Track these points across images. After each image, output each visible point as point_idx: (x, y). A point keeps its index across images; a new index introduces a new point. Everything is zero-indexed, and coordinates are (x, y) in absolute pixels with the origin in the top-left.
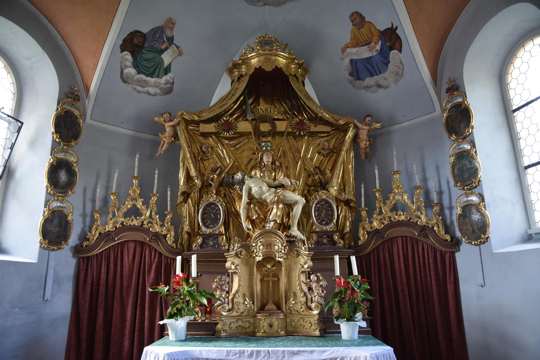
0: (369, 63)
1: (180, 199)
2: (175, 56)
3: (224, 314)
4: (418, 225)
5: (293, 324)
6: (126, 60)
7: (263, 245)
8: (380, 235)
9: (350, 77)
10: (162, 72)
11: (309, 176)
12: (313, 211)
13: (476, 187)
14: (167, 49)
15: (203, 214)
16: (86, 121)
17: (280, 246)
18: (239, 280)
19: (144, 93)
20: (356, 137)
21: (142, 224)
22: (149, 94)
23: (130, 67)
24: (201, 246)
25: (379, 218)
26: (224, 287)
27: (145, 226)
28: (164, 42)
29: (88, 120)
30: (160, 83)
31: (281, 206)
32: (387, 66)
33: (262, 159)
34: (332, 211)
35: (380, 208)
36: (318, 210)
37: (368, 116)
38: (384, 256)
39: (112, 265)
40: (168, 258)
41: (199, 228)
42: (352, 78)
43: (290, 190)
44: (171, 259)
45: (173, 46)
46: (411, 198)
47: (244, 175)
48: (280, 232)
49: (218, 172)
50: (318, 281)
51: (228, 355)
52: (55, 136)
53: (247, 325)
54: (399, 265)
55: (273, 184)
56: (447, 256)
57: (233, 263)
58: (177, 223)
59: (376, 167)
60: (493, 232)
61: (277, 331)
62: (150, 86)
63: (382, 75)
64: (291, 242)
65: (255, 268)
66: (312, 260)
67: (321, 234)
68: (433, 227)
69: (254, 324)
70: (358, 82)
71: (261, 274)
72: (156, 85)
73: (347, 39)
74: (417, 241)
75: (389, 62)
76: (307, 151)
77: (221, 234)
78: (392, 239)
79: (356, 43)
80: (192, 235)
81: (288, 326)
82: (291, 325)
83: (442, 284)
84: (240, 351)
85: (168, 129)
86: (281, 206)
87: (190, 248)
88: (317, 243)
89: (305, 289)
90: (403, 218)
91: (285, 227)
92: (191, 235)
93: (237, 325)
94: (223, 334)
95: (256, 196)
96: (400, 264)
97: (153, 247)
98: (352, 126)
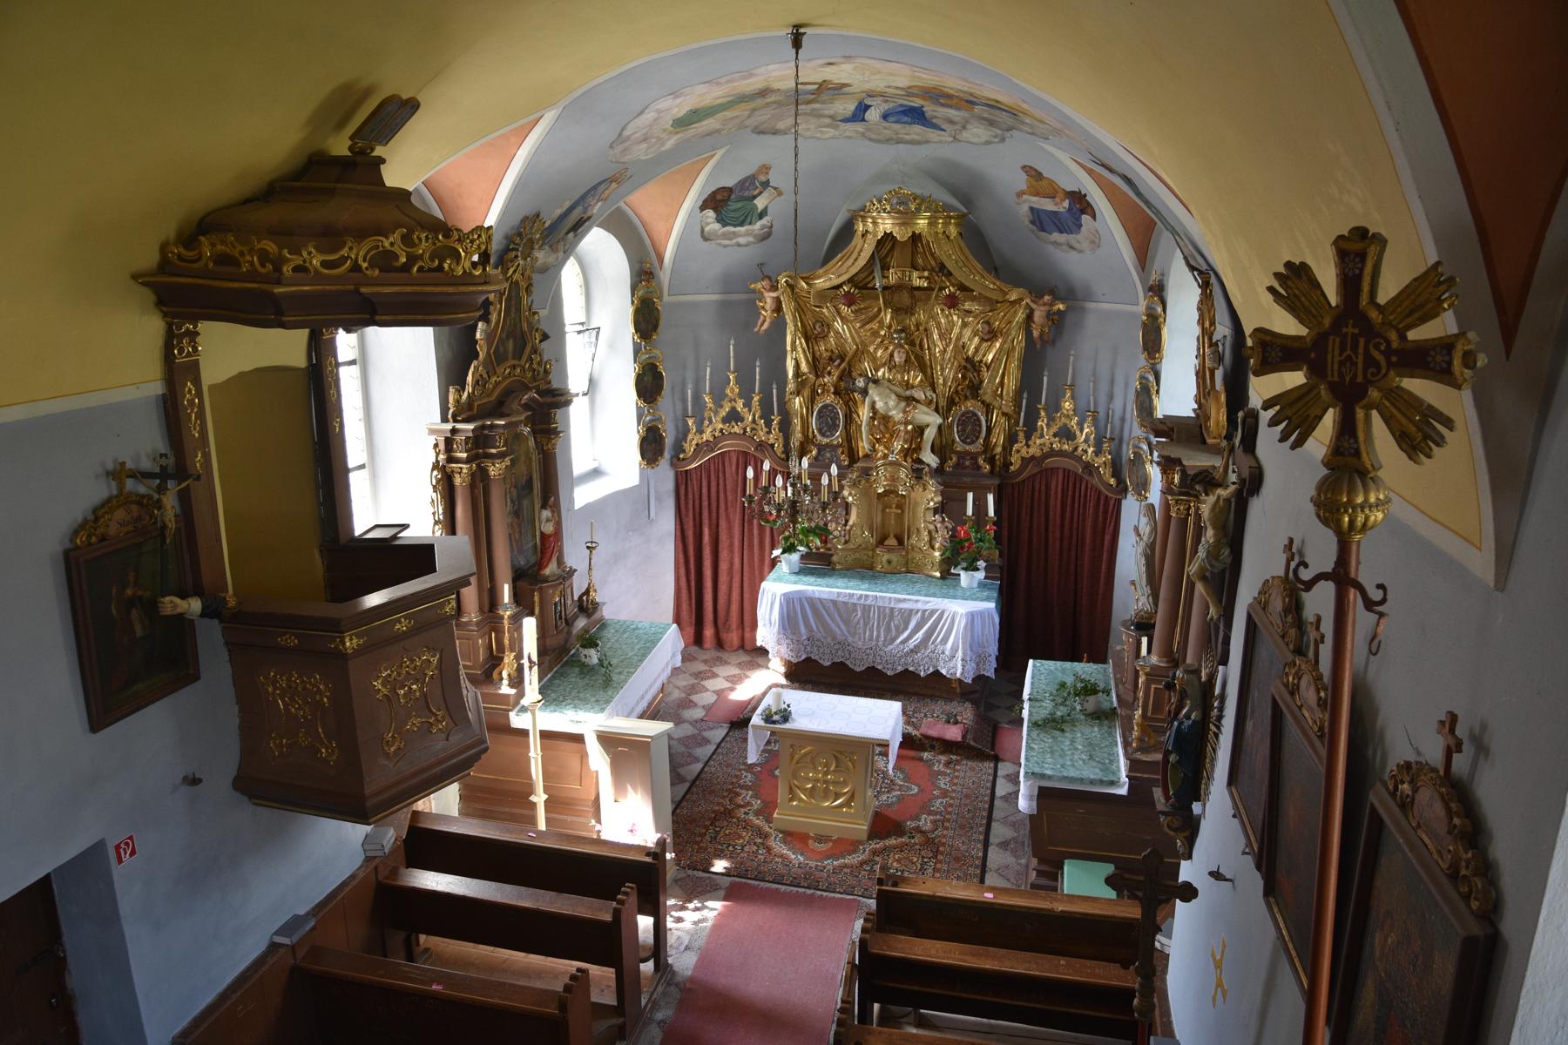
2: (772, 198)
3: (839, 547)
4: (1082, 460)
6: (708, 217)
9: (1030, 225)
14: (761, 193)
19: (733, 246)
21: (745, 431)
22: (739, 245)
28: (757, 187)
29: (666, 298)
30: (753, 231)
32: (1080, 229)
35: (1043, 429)
41: (814, 436)
42: (1034, 228)
51: (838, 596)
55: (903, 394)
56: (1112, 502)
62: (741, 236)
63: (1074, 236)
68: (1099, 467)
72: (747, 234)
74: (1081, 479)
78: (1052, 469)
84: (850, 594)
86: (910, 427)
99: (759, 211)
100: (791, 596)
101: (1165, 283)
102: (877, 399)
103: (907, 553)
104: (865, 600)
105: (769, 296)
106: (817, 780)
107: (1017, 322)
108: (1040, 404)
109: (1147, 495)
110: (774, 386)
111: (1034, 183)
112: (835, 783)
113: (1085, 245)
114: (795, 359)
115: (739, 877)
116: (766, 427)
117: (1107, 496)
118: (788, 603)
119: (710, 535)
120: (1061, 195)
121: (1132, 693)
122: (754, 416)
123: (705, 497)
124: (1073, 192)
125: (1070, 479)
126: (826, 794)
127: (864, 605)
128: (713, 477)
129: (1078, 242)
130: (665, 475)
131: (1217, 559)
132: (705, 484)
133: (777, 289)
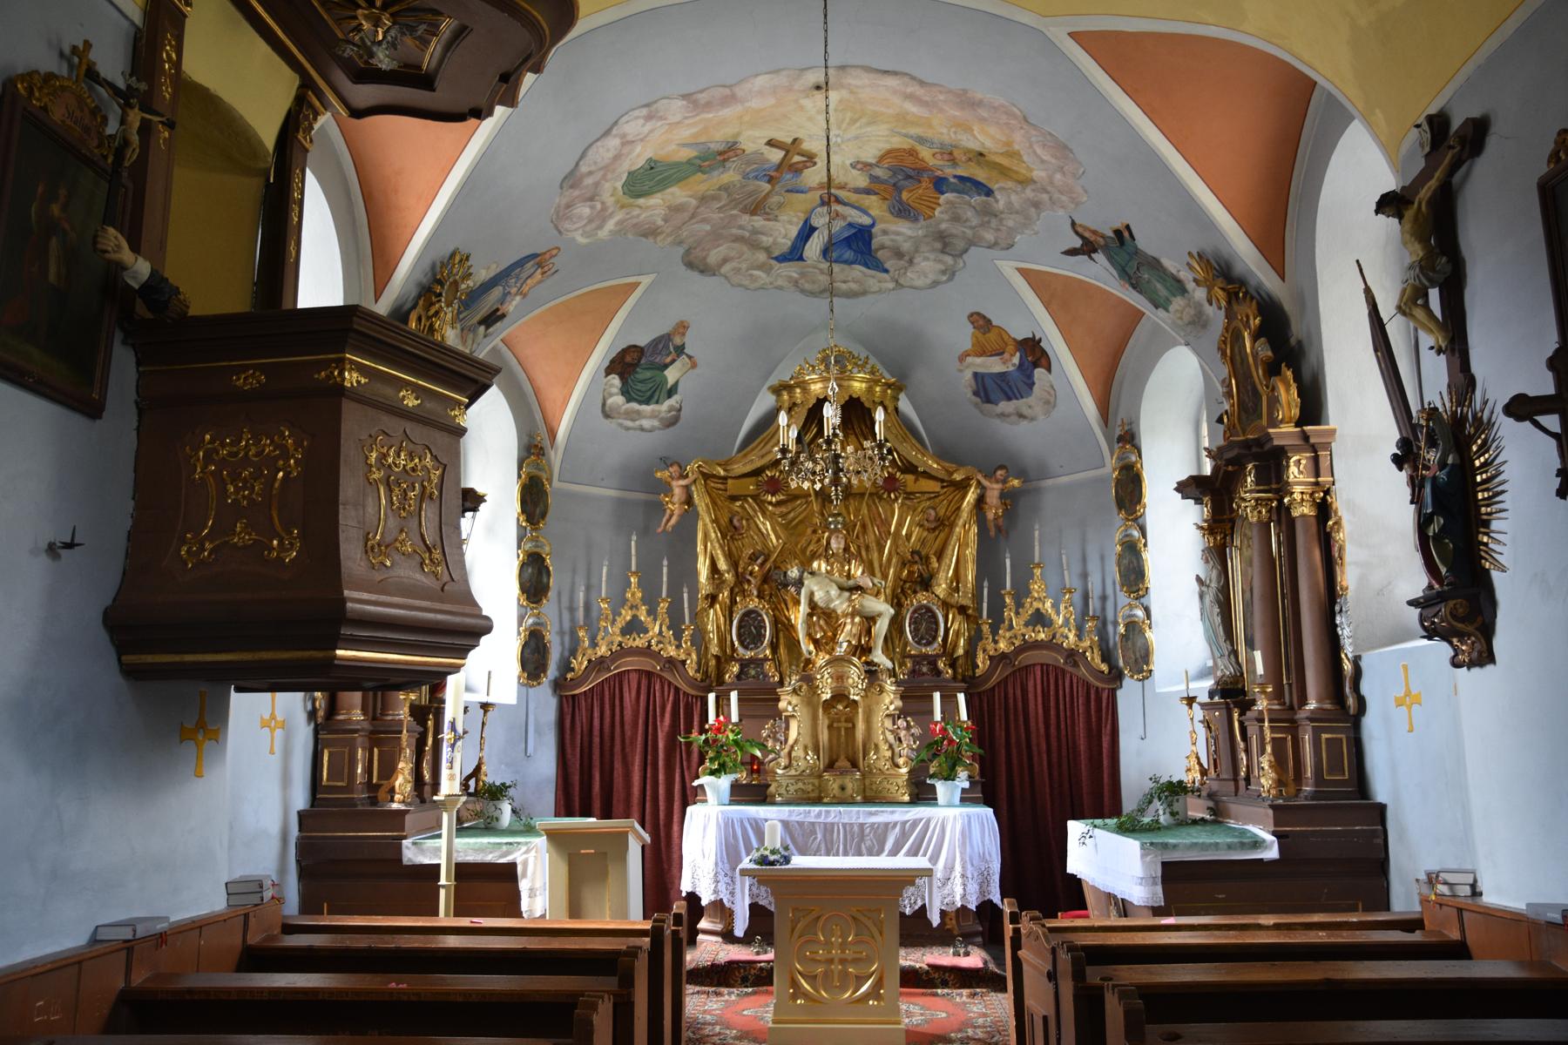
0: (1003, 381)
1: (702, 604)
3: (779, 771)
5: (874, 787)
6: (612, 386)
7: (832, 677)
8: (1008, 661)
9: (973, 398)
10: (664, 394)
11: (904, 564)
12: (907, 624)
13: (1143, 596)
14: (673, 361)
15: (740, 627)
16: (553, 484)
17: (856, 679)
18: (799, 726)
19: (634, 429)
20: (980, 501)
21: (650, 646)
22: (642, 429)
23: (617, 394)
24: (738, 677)
25: (1008, 635)
26: (778, 736)
27: (654, 648)
29: (556, 483)
30: (660, 412)
31: (857, 620)
32: (1031, 389)
33: (828, 543)
34: (937, 623)
35: (1011, 620)
36: (915, 623)
37: (1002, 467)
38: (1014, 693)
39: (607, 706)
40: (688, 694)
42: (978, 400)
43: (871, 595)
44: (693, 696)
45: (684, 356)
46: (1055, 606)
47: (803, 572)
48: (855, 660)
49: (759, 561)
50: (908, 727)
51: (789, 816)
52: (521, 519)
53: (810, 788)
54: (1036, 706)
56: (1105, 695)
57: (790, 703)
58: (700, 639)
59: (1008, 555)
60: (1158, 663)
61: (852, 796)
62: (645, 417)
63: (1024, 400)
64: (872, 673)
65: (821, 710)
66: (902, 698)
67: (919, 659)
69: (820, 786)
70: (989, 406)
71: (829, 718)
72: (653, 416)
73: (967, 345)
74: (1063, 671)
75: (1034, 384)
76: (900, 525)
77: (766, 659)
78: (1027, 666)
79: (982, 352)
80: (723, 660)
81: (867, 790)
82: (871, 789)
83: (1094, 737)
85: (677, 492)
86: (857, 620)
87: (721, 681)
88: (913, 672)
89: (891, 738)
90: (1042, 636)
91: (863, 650)
92: (722, 661)
93: (796, 787)
94: (778, 799)
95: (821, 604)
96: (1036, 705)
97: (666, 679)
98: (974, 483)
99: (669, 386)
100: (730, 815)
101: (1135, 430)
102: (815, 588)
104: (826, 817)
105: (677, 487)
106: (831, 961)
108: (1005, 588)
109: (1152, 667)
110: (685, 590)
111: (980, 336)
112: (856, 961)
113: (1038, 410)
114: (707, 557)
116: (675, 639)
117: (1097, 688)
118: (726, 825)
120: (1010, 348)
121: (1232, 783)
124: (1025, 339)
126: (846, 981)
127: (825, 824)
129: (1030, 407)
130: (545, 703)
131: (1433, 269)
132: (596, 714)
133: (687, 476)
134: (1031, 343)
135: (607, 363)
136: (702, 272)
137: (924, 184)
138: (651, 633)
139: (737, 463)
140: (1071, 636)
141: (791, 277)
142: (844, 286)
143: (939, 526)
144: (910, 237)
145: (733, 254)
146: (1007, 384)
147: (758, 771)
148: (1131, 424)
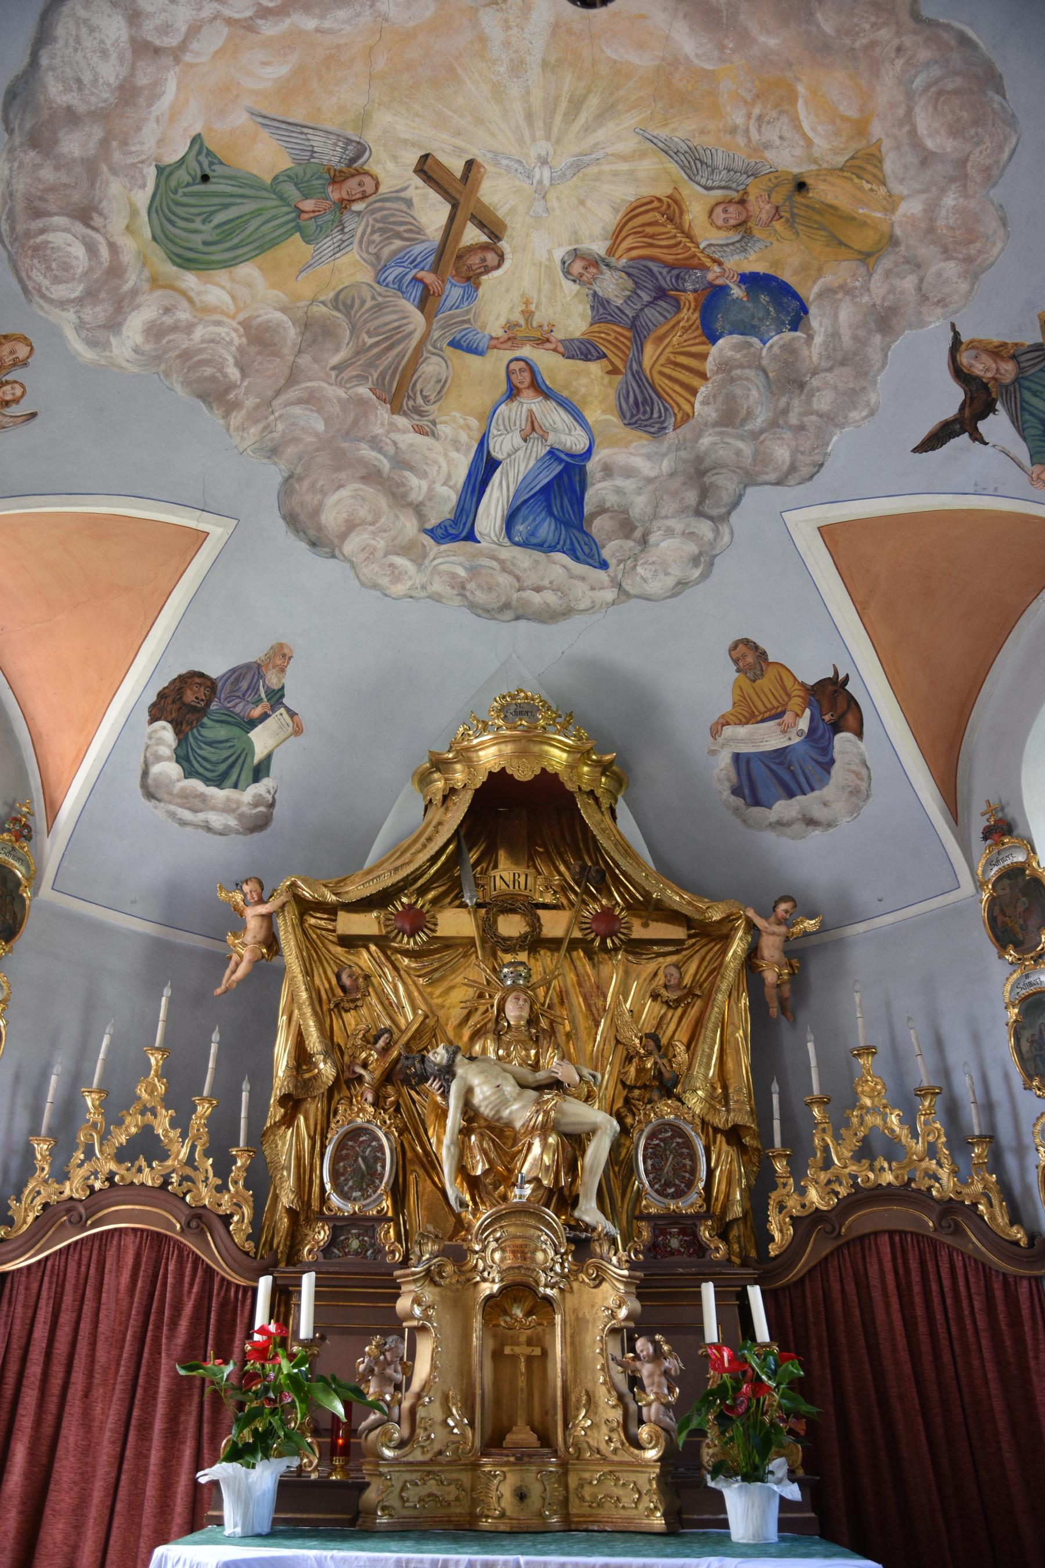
0: (781, 764)
1: (276, 1113)
3: (388, 1453)
4: (932, 1198)
6: (160, 741)
10: (247, 774)
12: (640, 1158)
14: (264, 717)
15: (336, 1159)
17: (551, 1253)
19: (196, 826)
20: (753, 953)
21: (166, 1183)
22: (208, 829)
23: (168, 759)
24: (327, 1250)
25: (823, 1177)
29: (46, 891)
30: (239, 803)
31: (552, 1140)
33: (501, 1009)
34: (693, 1157)
35: (826, 1149)
36: (654, 1155)
38: (843, 1291)
40: (229, 1283)
42: (739, 802)
44: (238, 1286)
45: (282, 710)
46: (909, 1120)
49: (381, 1043)
50: (658, 1355)
56: (1024, 1289)
57: (417, 1301)
61: (540, 1515)
62: (213, 808)
63: (816, 793)
66: (640, 1297)
67: (663, 1223)
68: (975, 1205)
71: (495, 1336)
72: (227, 808)
73: (725, 704)
74: (934, 1243)
75: (832, 761)
78: (862, 1238)
81: (574, 1501)
82: (582, 1499)
86: (552, 1140)
88: (653, 1249)
90: (888, 1177)
93: (423, 1491)
95: (486, 1111)
96: (888, 1314)
99: (256, 761)
103: (564, 1466)
107: (735, 952)
115: (122, 1347)
119: (28, 1475)
120: (795, 703)
122: (193, 1148)
123: (36, 1354)
125: (911, 1256)
128: (68, 1299)
134: (831, 688)
135: (152, 698)
136: (313, 544)
137: (684, 314)
138: (169, 1162)
139: (353, 883)
140: (944, 1173)
141: (454, 576)
142: (536, 598)
143: (686, 996)
144: (649, 481)
145: (363, 513)
146: (789, 768)
147: (345, 1451)
148: (1002, 809)
